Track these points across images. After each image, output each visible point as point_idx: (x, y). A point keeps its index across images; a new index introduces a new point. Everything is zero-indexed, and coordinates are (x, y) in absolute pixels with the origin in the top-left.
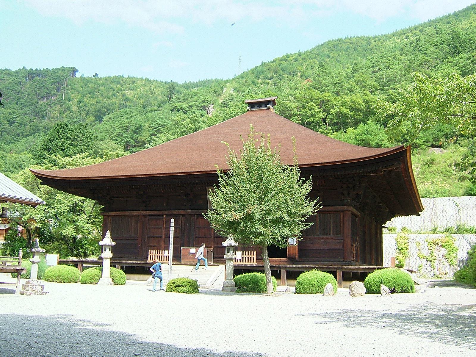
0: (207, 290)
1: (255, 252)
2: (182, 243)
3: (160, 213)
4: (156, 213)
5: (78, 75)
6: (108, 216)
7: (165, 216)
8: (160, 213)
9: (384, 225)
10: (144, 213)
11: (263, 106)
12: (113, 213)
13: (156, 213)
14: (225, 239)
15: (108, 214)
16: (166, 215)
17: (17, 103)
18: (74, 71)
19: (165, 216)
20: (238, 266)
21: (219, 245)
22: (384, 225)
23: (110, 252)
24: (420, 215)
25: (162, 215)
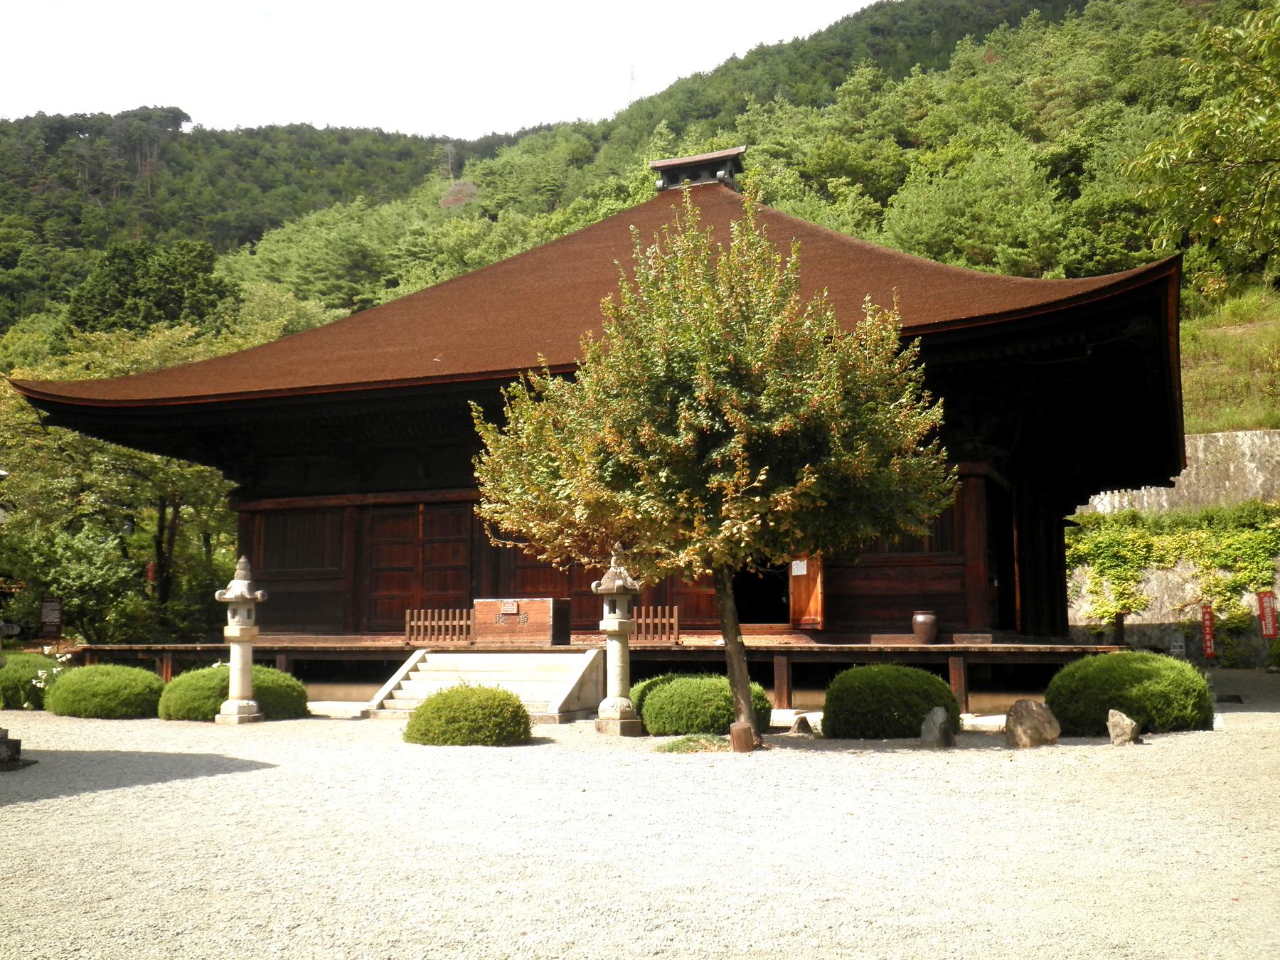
0: (418, 287)
1: (676, 608)
2: (140, 656)
3: (408, 497)
4: (394, 498)
5: (186, 128)
6: (254, 513)
7: (421, 507)
8: (408, 497)
9: (1070, 518)
10: (357, 499)
11: (705, 174)
12: (266, 504)
13: (394, 498)
14: (598, 574)
15: (252, 505)
16: (427, 504)
17: (22, 211)
18: (177, 116)
19: (421, 507)
20: (644, 652)
21: (584, 589)
22: (1070, 518)
23: (252, 621)
24: (1172, 485)
25: (414, 505)
